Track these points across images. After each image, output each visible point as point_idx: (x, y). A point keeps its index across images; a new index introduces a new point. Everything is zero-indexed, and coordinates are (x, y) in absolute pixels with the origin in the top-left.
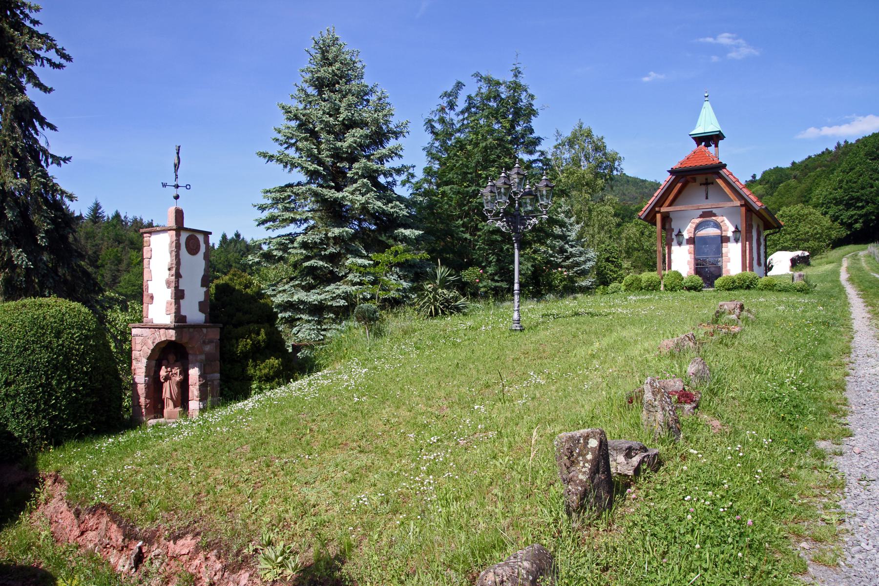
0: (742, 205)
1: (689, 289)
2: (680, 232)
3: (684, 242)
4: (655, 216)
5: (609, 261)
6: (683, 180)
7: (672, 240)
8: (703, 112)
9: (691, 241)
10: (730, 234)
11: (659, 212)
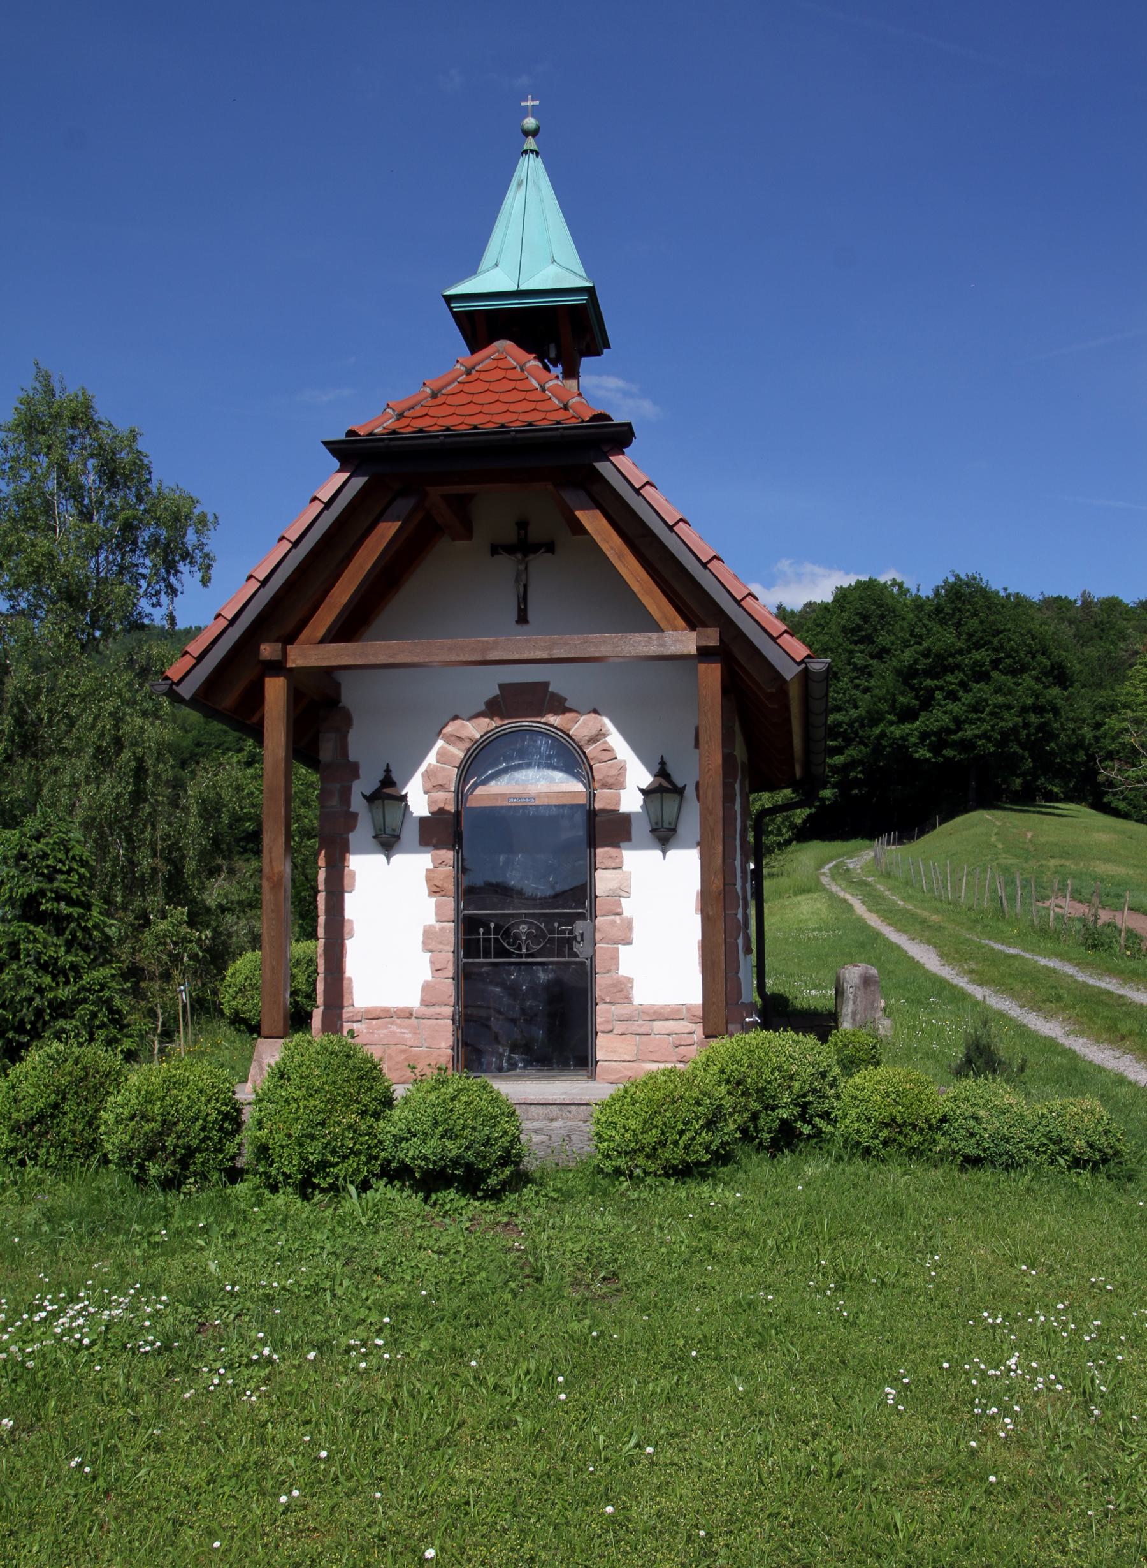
0: (704, 653)
1: (430, 1181)
2: (388, 781)
3: (411, 833)
4: (255, 697)
5: (40, 918)
6: (404, 505)
7: (351, 820)
8: (514, 201)
9: (443, 830)
10: (631, 802)
11: (277, 667)
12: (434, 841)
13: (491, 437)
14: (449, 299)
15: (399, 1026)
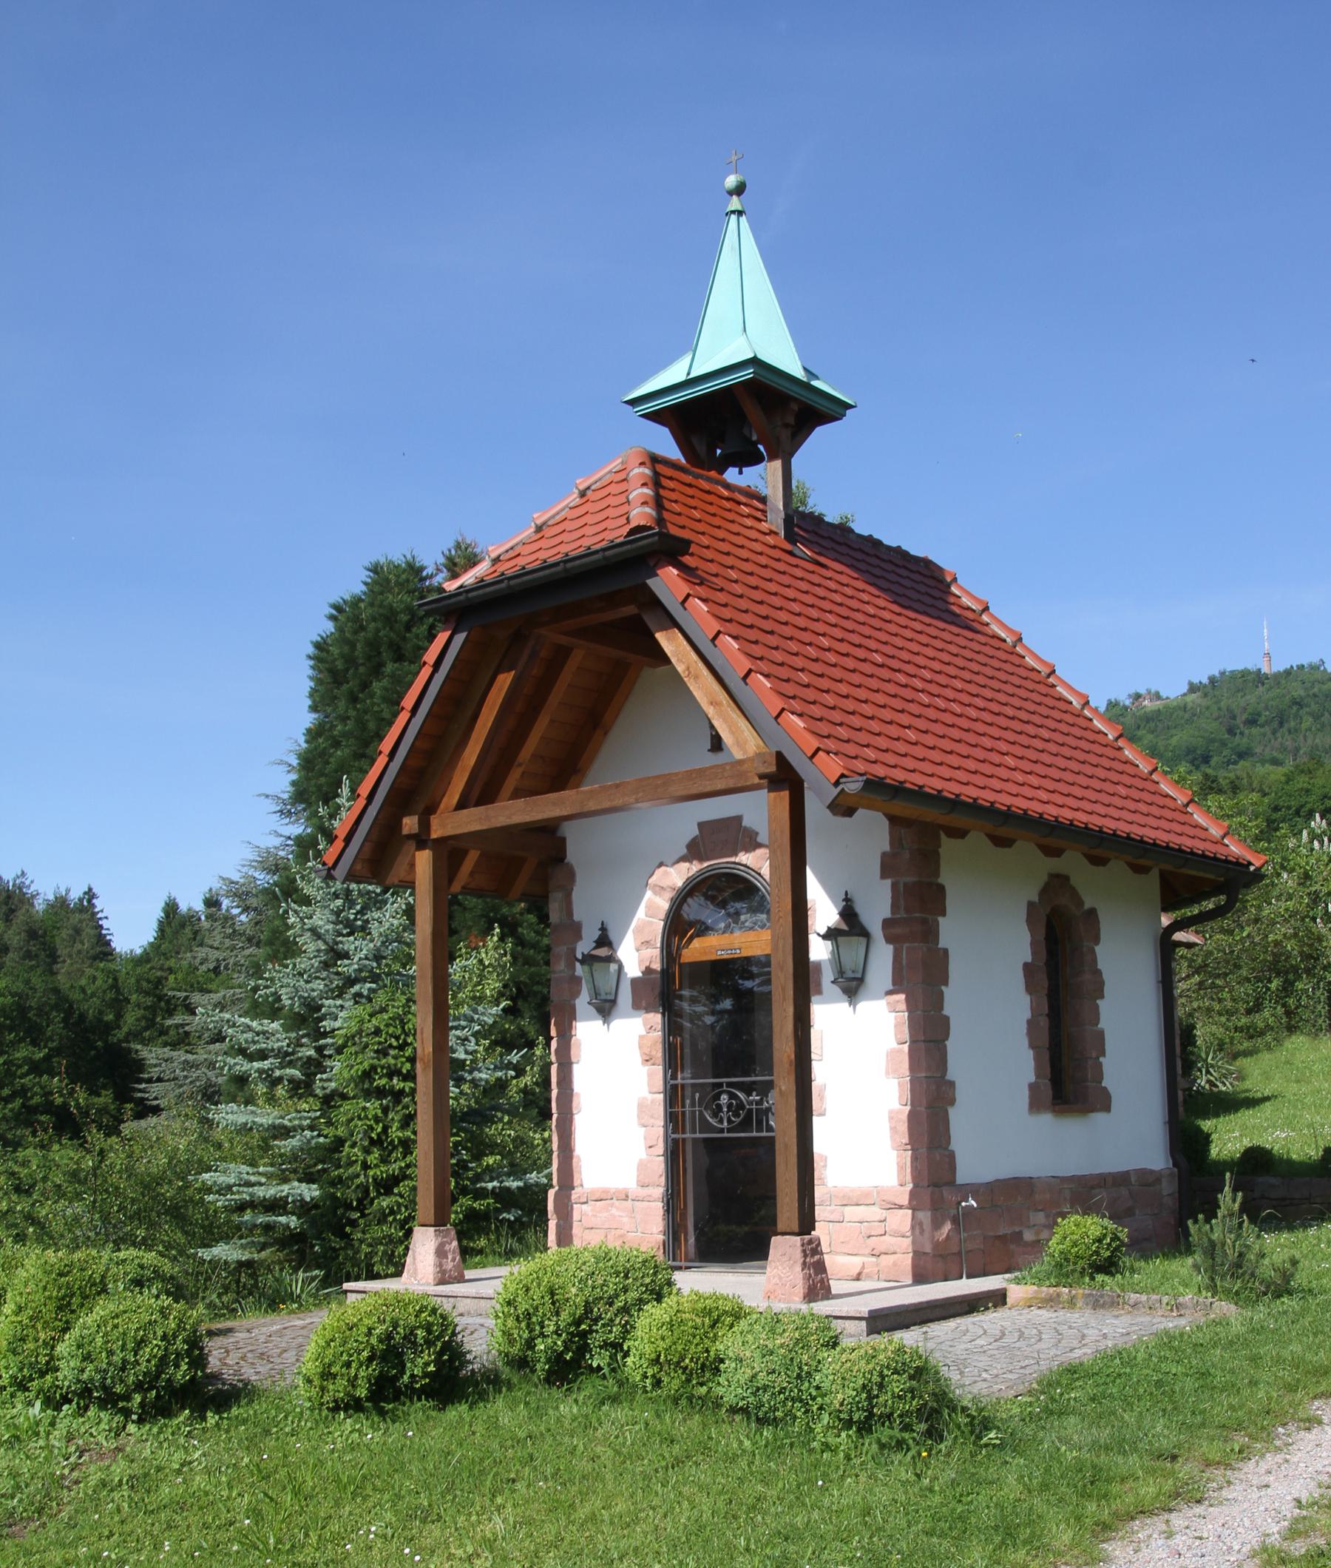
3: (625, 996)
12: (644, 1004)
13: (541, 574)
14: (633, 403)
15: (618, 1209)
